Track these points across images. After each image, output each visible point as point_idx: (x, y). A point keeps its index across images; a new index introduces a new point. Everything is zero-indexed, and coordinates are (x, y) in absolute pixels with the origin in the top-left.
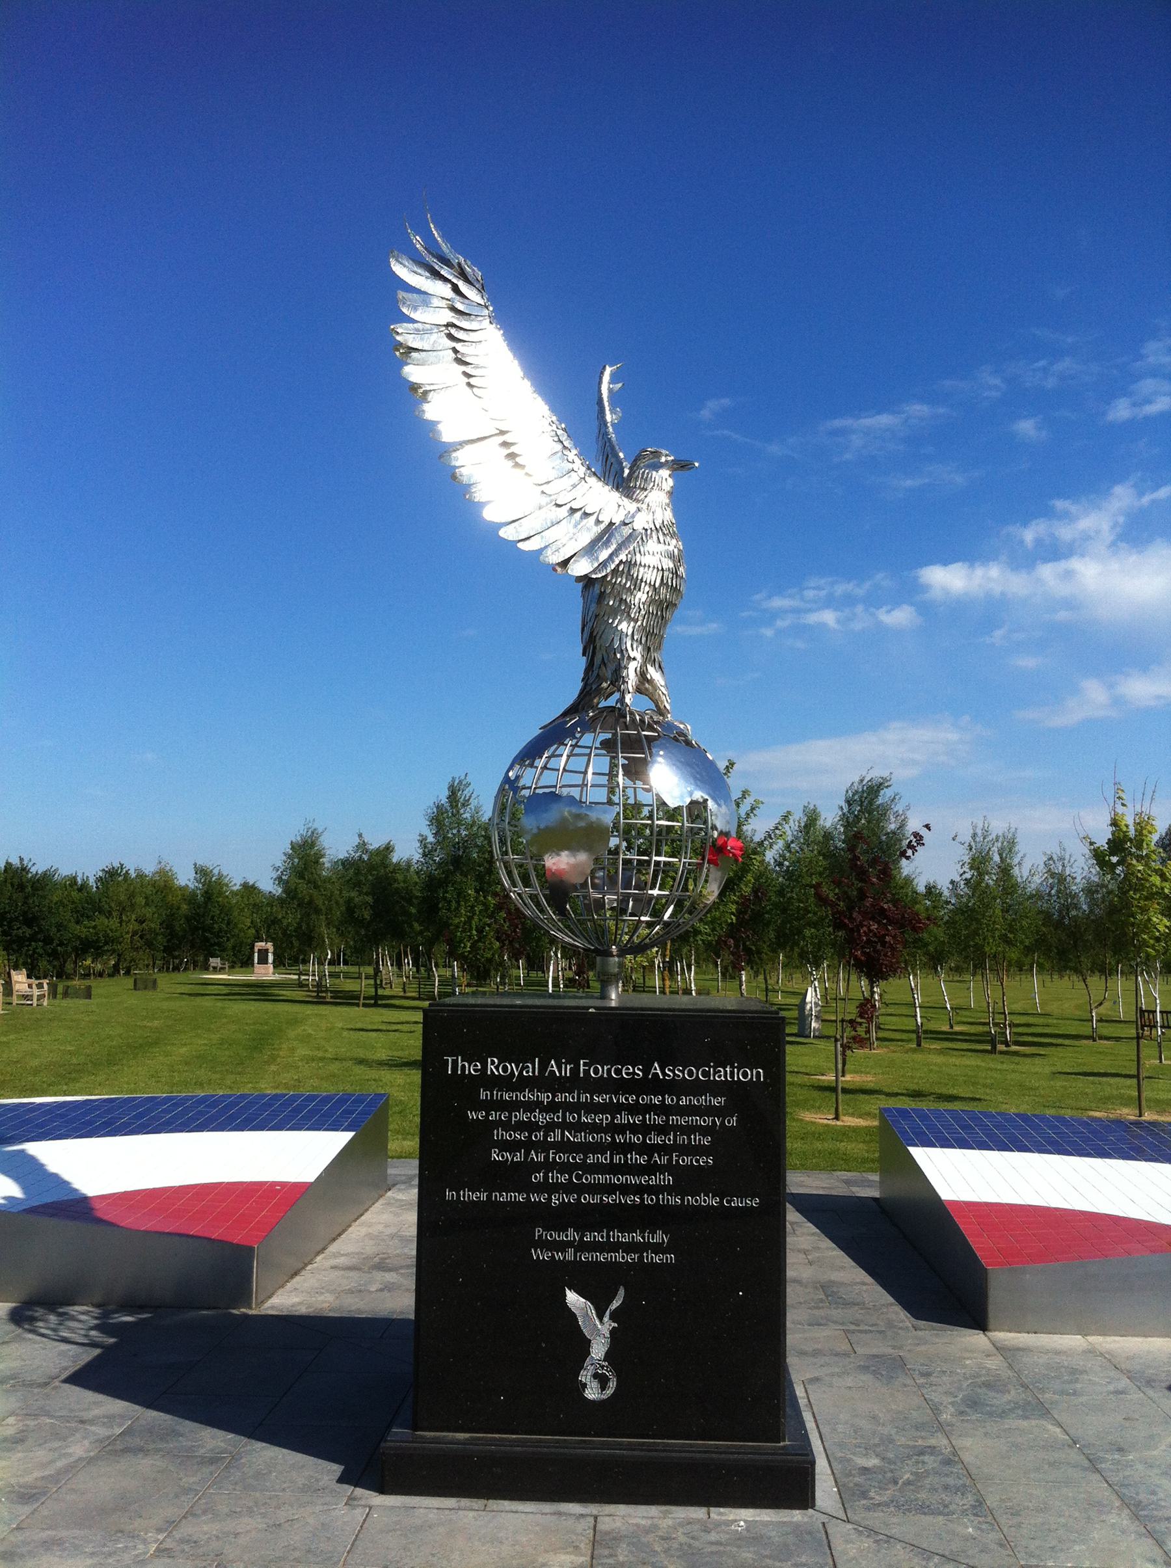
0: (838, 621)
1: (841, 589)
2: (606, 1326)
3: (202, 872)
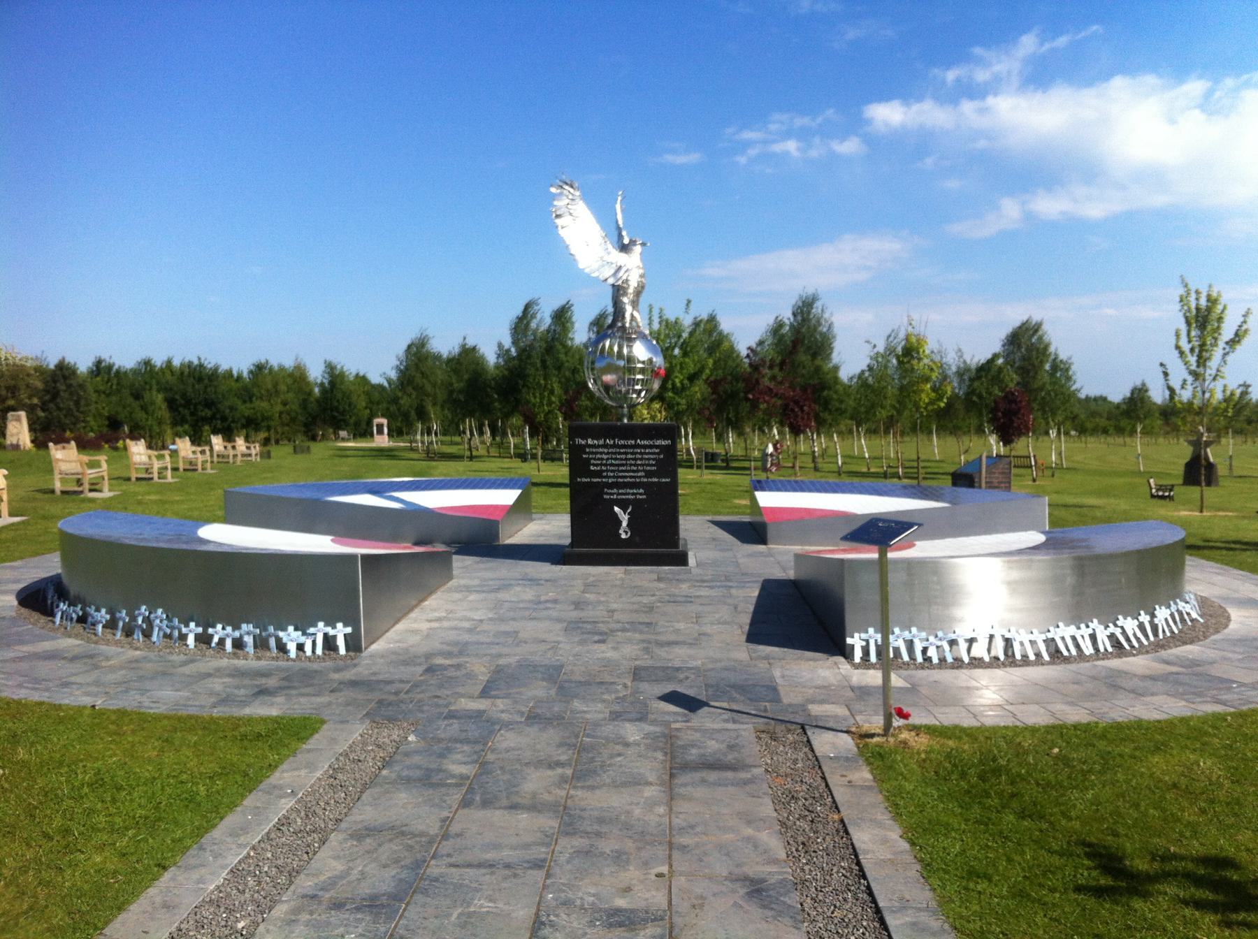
0: (798, 149)
1: (800, 121)
2: (626, 517)
3: (330, 367)
